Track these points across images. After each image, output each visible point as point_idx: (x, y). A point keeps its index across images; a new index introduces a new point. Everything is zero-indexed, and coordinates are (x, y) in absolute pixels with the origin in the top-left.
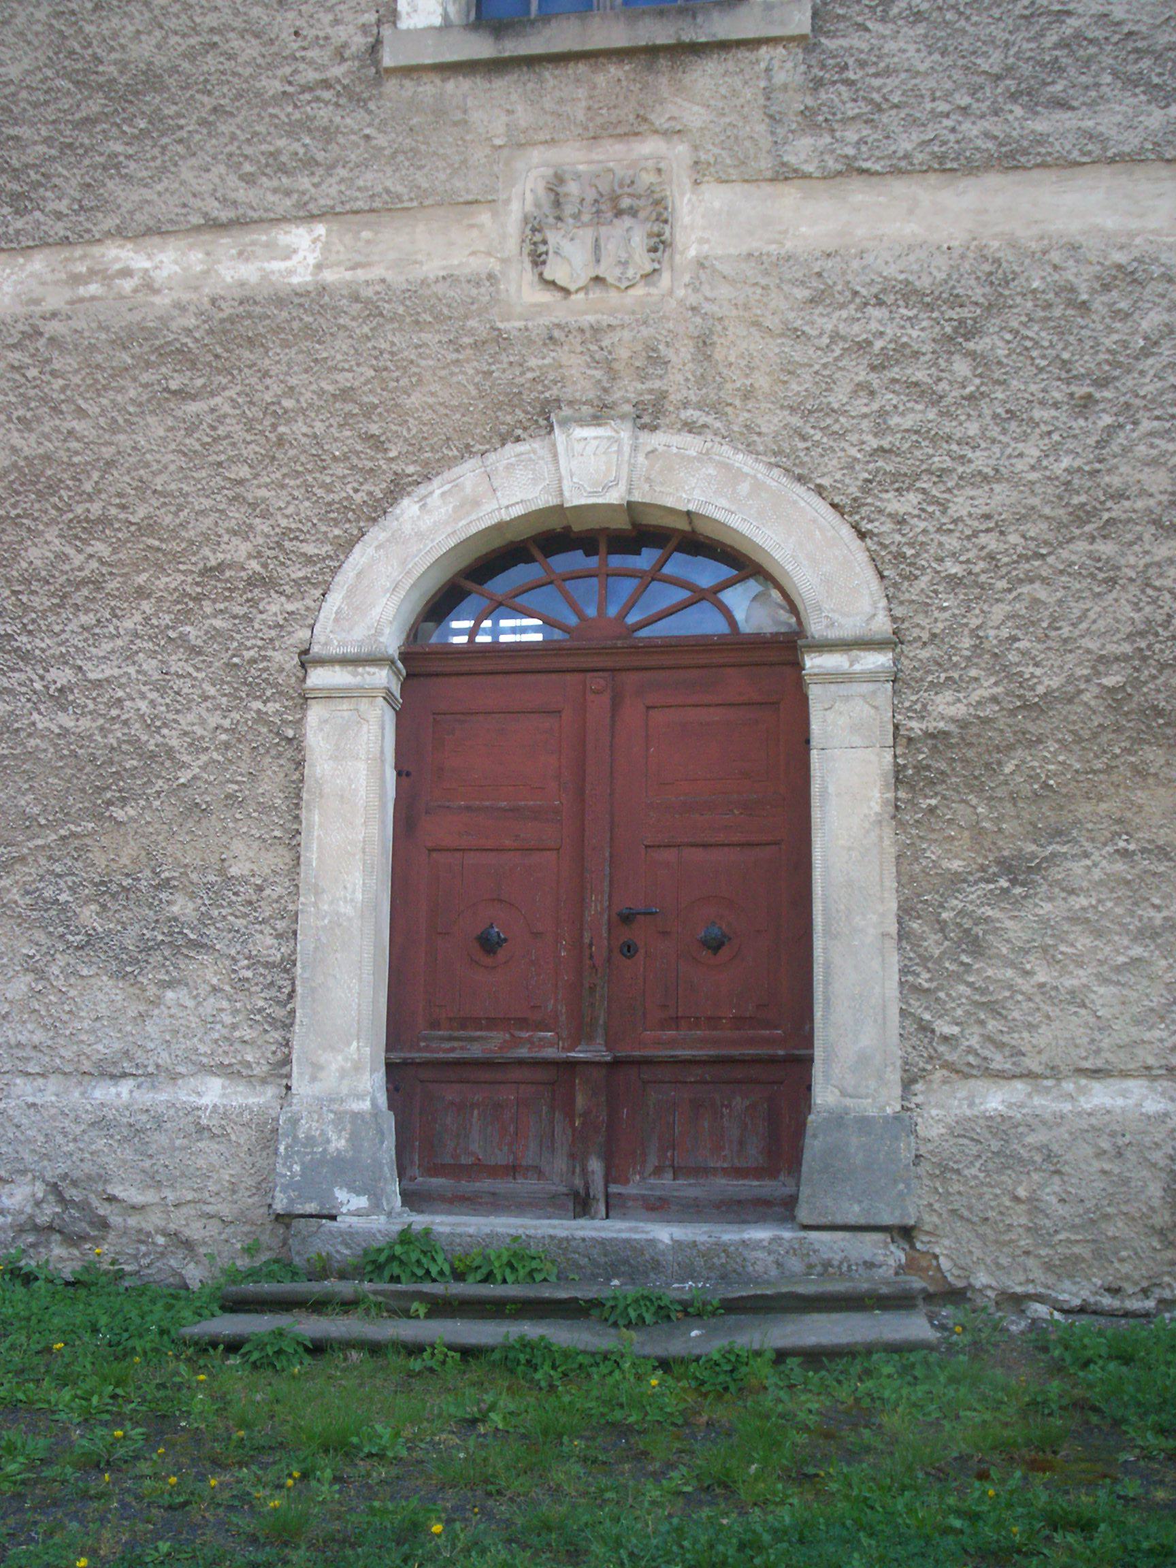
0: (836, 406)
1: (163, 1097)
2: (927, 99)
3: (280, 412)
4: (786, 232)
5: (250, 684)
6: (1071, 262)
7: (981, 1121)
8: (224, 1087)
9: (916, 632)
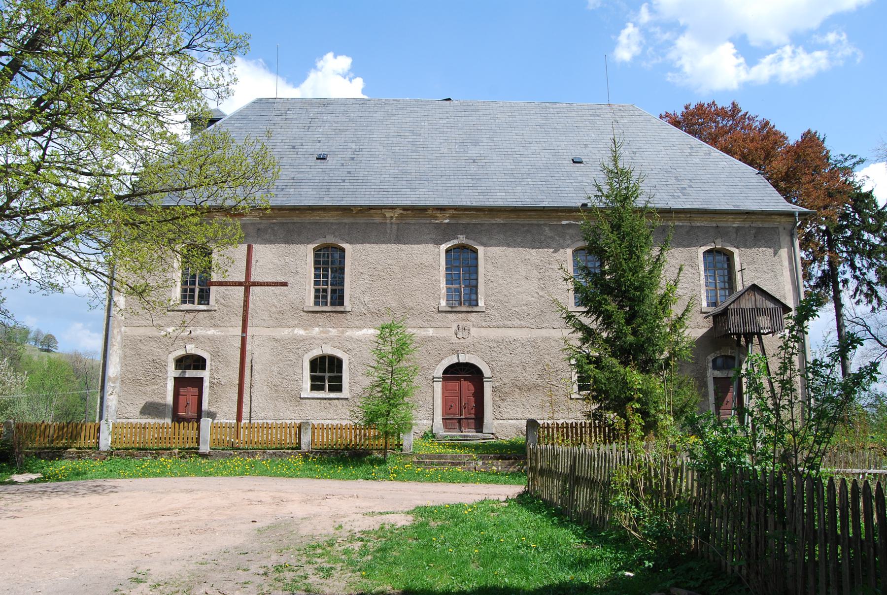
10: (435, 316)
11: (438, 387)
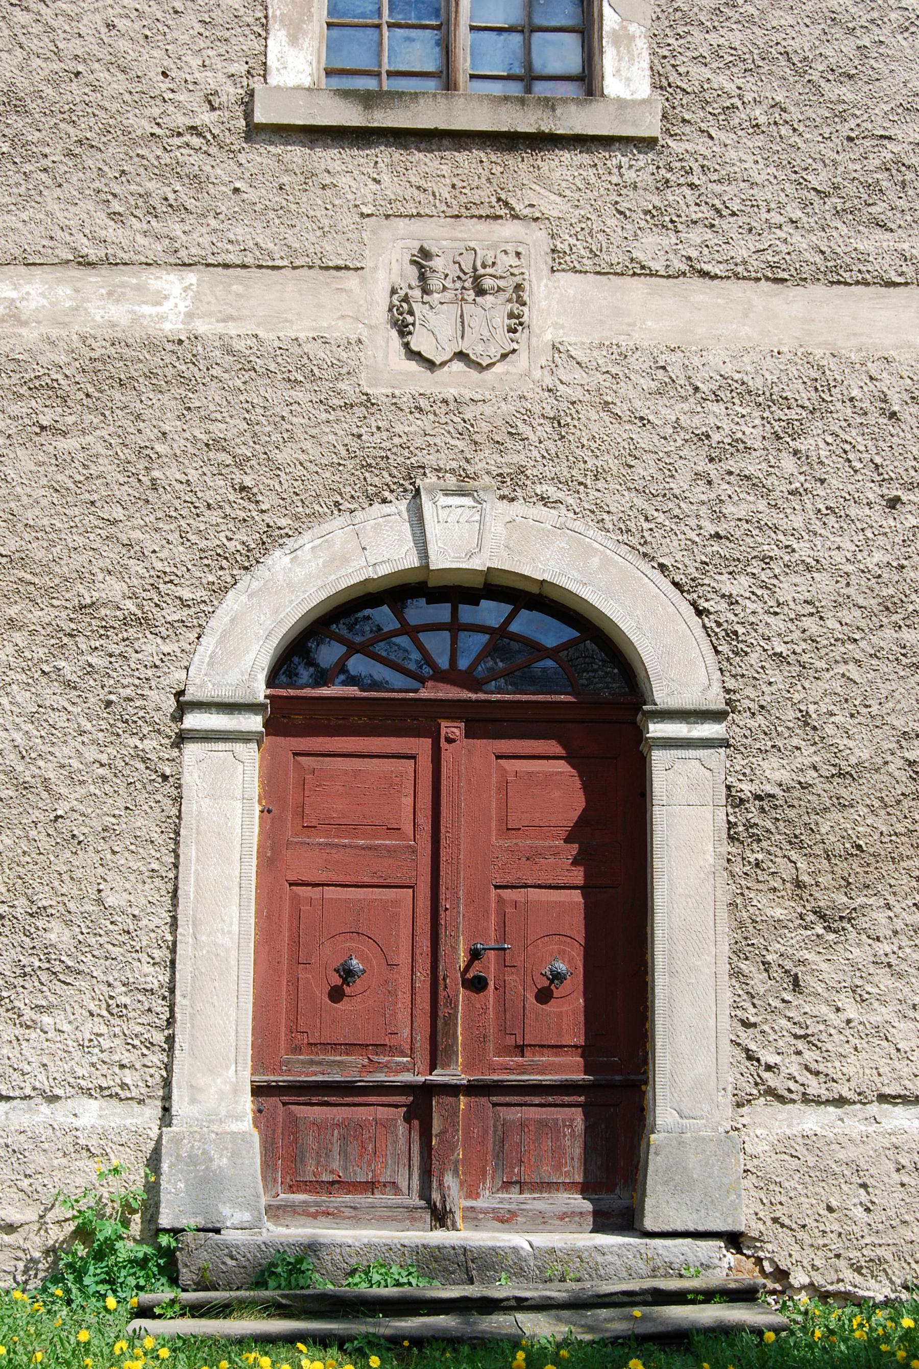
0: (677, 492)
1: (39, 1118)
2: (763, 210)
3: (154, 456)
4: (634, 324)
5: (126, 722)
6: (885, 374)
7: (800, 1140)
8: (101, 1109)
9: (746, 703)
10: (221, 170)
11: (226, 790)
